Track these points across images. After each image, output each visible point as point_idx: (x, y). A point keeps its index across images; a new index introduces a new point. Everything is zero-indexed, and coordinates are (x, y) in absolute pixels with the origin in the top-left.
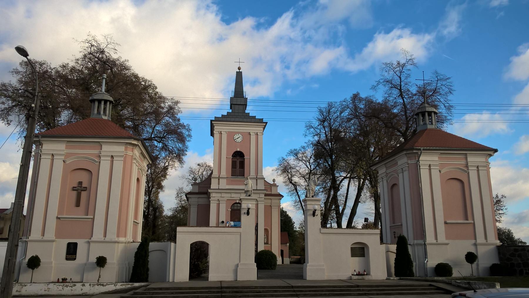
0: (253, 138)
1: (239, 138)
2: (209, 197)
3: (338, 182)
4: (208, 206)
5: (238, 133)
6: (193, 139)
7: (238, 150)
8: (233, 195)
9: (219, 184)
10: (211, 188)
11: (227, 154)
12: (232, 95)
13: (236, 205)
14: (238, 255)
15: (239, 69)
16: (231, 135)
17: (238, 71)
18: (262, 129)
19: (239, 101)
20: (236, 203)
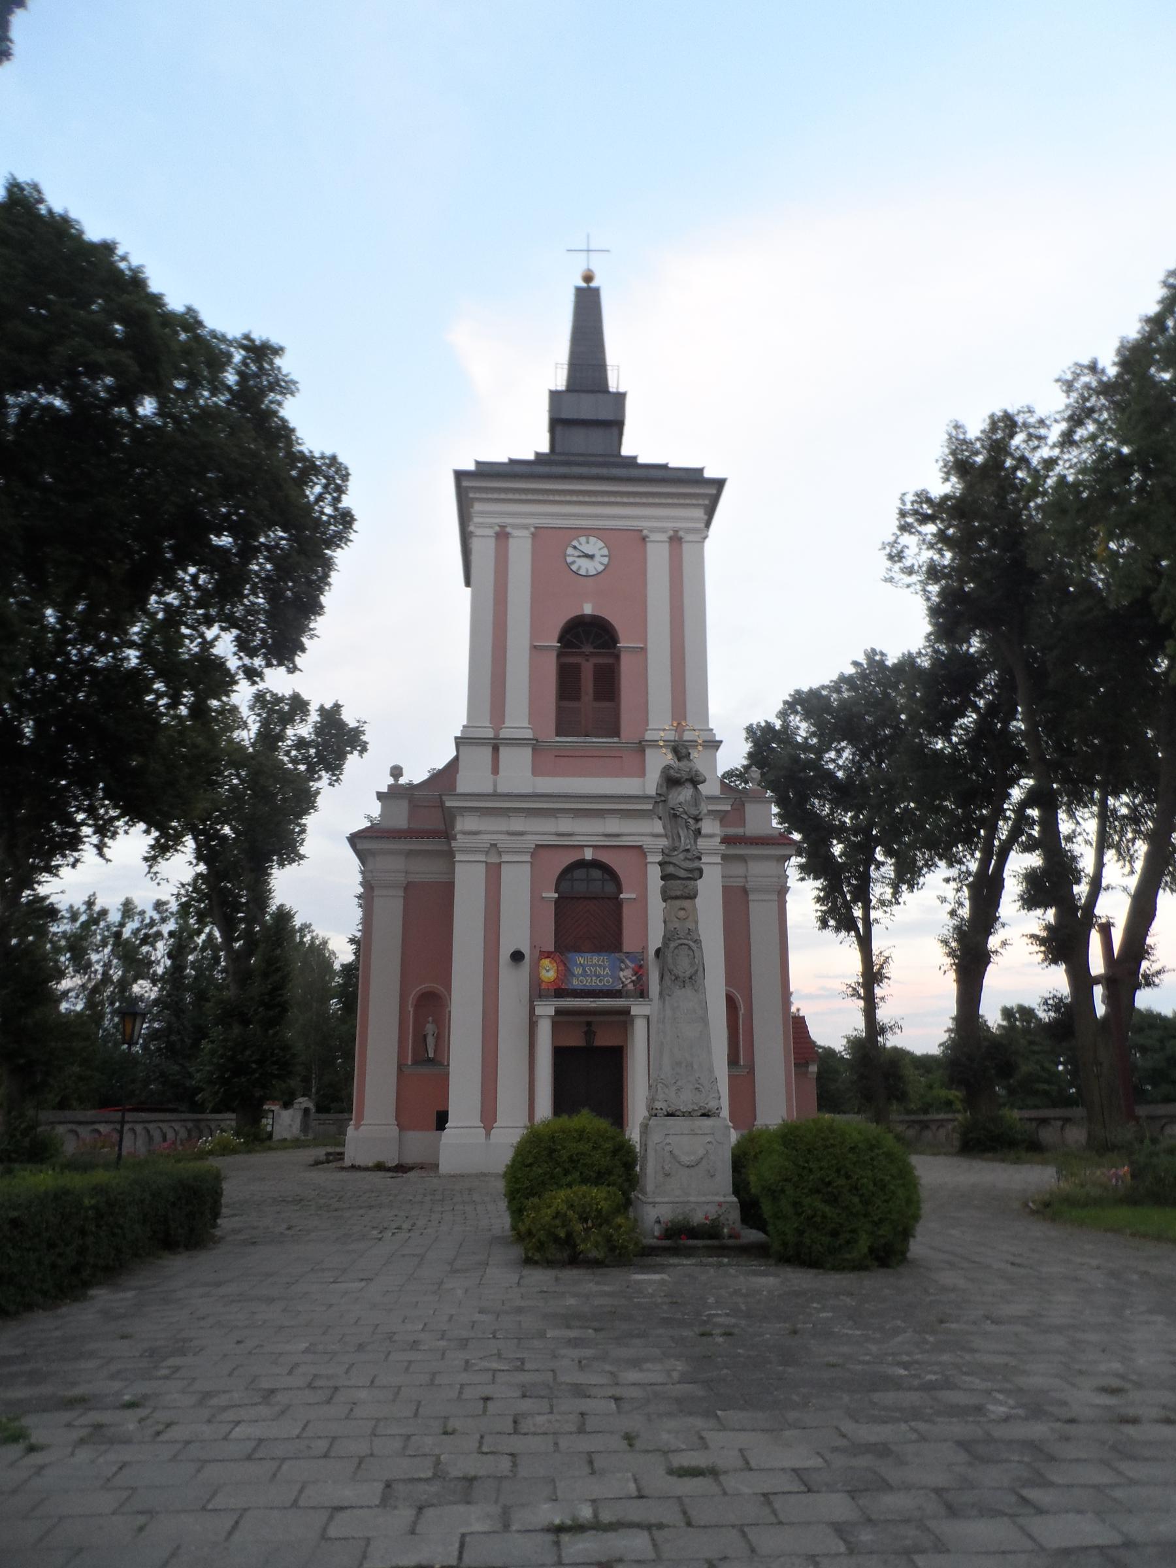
0: (657, 555)
1: (591, 557)
2: (452, 864)
3: (876, 968)
4: (447, 890)
5: (588, 532)
6: (360, 534)
7: (588, 609)
8: (565, 825)
9: (495, 770)
10: (460, 789)
11: (536, 630)
12: (560, 381)
13: (579, 873)
14: (475, 558)
15: (588, 278)
16: (550, 544)
17: (584, 285)
18: (700, 513)
19: (586, 408)
20: (581, 864)
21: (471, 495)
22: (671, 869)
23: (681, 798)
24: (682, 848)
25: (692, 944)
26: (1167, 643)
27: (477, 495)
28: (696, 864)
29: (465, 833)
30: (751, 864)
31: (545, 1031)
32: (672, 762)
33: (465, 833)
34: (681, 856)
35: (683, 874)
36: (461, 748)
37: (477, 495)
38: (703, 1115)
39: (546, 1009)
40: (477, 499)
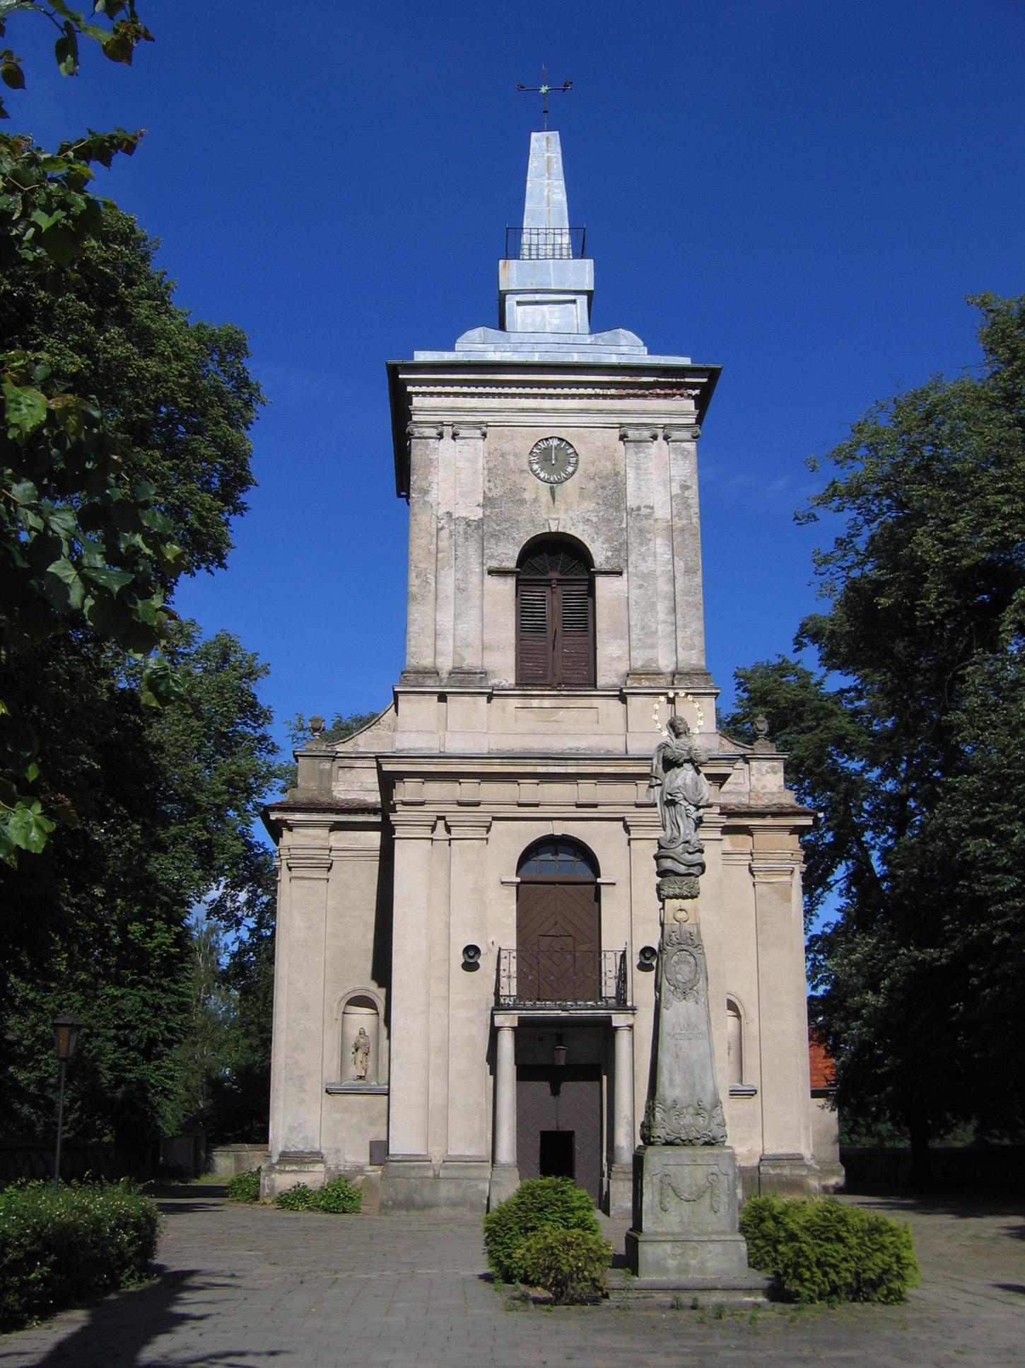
21: (410, 389)
22: (668, 864)
23: (679, 782)
24: (681, 840)
25: (691, 949)
26: (588, 264)
27: (417, 389)
28: (696, 858)
29: (404, 804)
30: (758, 836)
31: (507, 1043)
32: (668, 740)
33: (404, 804)
34: (680, 849)
35: (682, 869)
36: (385, 1138)
37: (417, 389)
38: (706, 1143)
39: (507, 1021)
40: (417, 394)
